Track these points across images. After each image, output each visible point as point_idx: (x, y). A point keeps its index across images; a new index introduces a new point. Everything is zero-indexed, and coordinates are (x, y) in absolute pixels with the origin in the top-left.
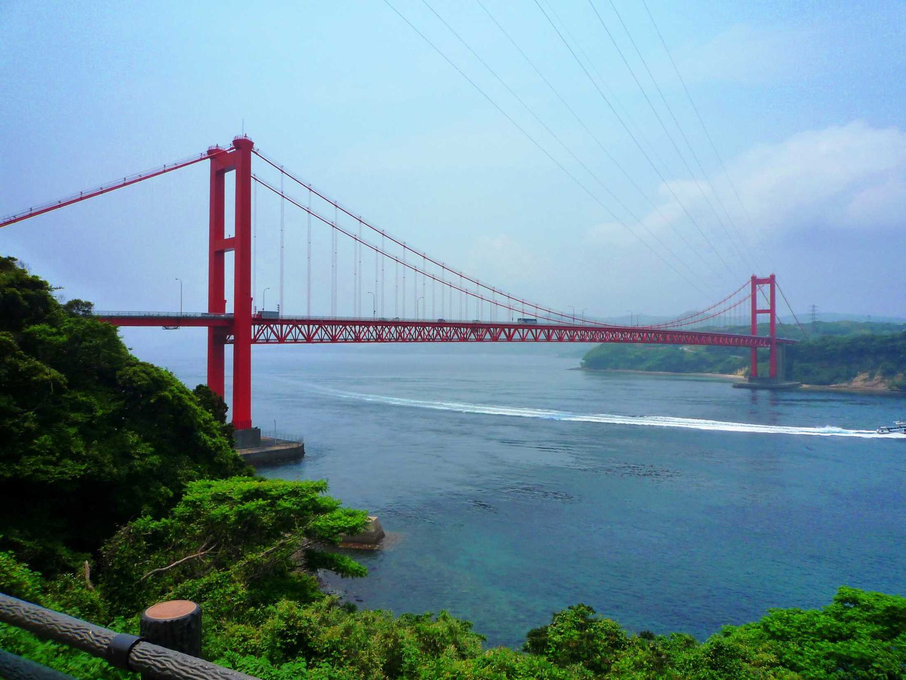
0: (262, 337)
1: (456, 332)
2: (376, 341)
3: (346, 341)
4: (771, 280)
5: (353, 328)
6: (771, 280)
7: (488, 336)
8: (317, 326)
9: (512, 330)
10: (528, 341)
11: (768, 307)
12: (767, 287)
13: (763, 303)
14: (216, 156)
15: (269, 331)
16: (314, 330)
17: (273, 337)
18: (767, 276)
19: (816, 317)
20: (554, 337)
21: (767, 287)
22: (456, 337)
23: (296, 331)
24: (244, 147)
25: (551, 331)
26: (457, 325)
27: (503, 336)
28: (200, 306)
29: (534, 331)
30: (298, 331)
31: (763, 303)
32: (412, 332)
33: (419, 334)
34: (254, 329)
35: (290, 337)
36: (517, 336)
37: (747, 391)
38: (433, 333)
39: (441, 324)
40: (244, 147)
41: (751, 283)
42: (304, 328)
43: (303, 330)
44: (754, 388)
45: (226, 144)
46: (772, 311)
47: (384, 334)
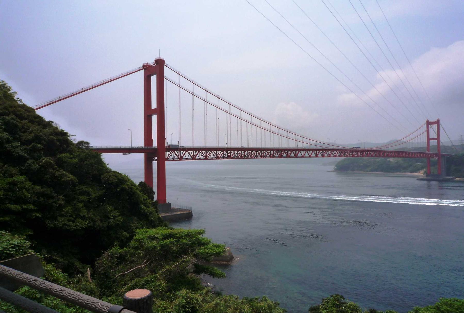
0: (171, 158)
1: (268, 153)
3: (212, 158)
4: (438, 123)
5: (216, 152)
6: (438, 123)
8: (197, 152)
9: (297, 152)
10: (306, 157)
12: (435, 126)
13: (433, 135)
17: (176, 157)
18: (435, 120)
20: (320, 155)
21: (435, 126)
24: (160, 63)
25: (318, 152)
27: (292, 155)
30: (188, 154)
31: (433, 135)
32: (255, 154)
33: (249, 155)
34: (167, 153)
35: (184, 157)
36: (300, 155)
38: (256, 154)
40: (160, 63)
42: (191, 153)
43: (190, 153)
46: (438, 139)
47: (232, 155)
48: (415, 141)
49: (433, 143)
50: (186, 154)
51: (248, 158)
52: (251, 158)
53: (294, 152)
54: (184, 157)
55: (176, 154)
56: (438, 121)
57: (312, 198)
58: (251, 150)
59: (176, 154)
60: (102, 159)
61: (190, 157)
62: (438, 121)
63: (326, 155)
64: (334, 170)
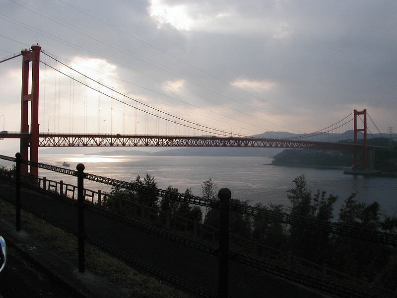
0: (90, 144)
1: (213, 142)
2: (166, 146)
3: (141, 146)
4: (364, 112)
5: (145, 140)
6: (364, 112)
7: (236, 144)
8: (128, 139)
9: (254, 142)
10: (267, 147)
11: (363, 128)
12: (362, 116)
13: (360, 126)
14: (24, 53)
15: (93, 140)
16: (126, 141)
17: (95, 143)
18: (363, 110)
19: (392, 131)
20: (273, 145)
21: (362, 116)
22: (221, 144)
23: (118, 141)
24: (37, 50)
25: (247, 142)
26: (221, 139)
27: (243, 144)
28: (17, 128)
29: (258, 142)
30: (119, 141)
31: (360, 126)
32: (192, 142)
33: (196, 143)
34: (41, 139)
35: (103, 144)
36: (256, 144)
37: (351, 176)
38: (202, 142)
39: (214, 138)
40: (37, 50)
41: (353, 114)
42: (122, 140)
43: (121, 140)
44: (355, 175)
45: (29, 48)
46: (365, 130)
47: (170, 143)
48: (340, 131)
49: (360, 136)
50: (117, 141)
51: (194, 146)
52: (198, 146)
53: (251, 142)
54: (103, 144)
55: (94, 140)
56: (365, 111)
57: (134, 166)
58: (189, 138)
59: (94, 140)
60: (246, 203)
61: (120, 143)
62: (365, 111)
63: (279, 145)
64: (271, 163)
